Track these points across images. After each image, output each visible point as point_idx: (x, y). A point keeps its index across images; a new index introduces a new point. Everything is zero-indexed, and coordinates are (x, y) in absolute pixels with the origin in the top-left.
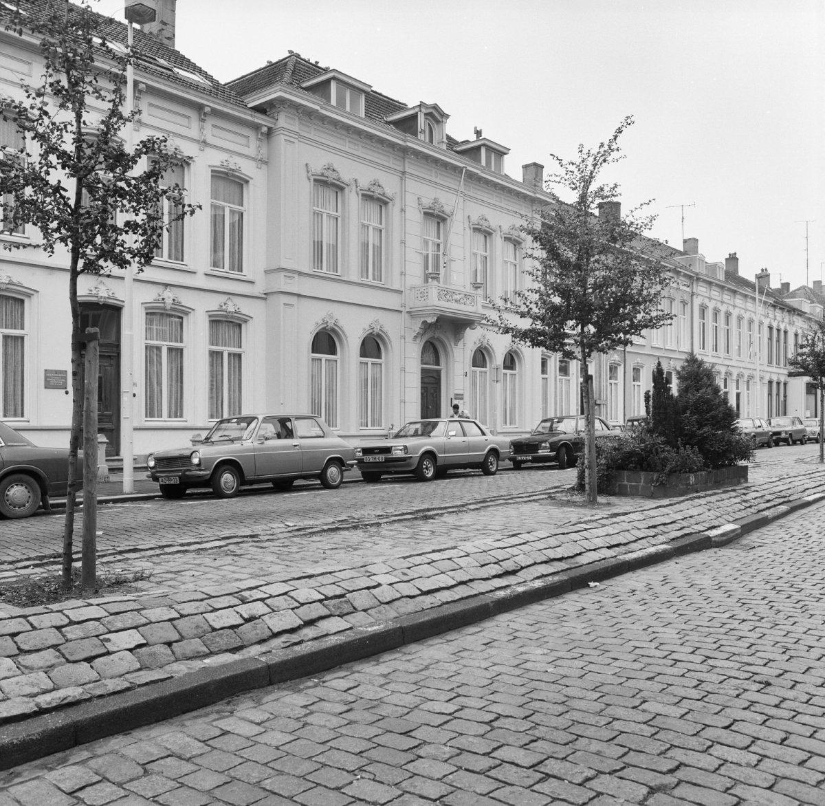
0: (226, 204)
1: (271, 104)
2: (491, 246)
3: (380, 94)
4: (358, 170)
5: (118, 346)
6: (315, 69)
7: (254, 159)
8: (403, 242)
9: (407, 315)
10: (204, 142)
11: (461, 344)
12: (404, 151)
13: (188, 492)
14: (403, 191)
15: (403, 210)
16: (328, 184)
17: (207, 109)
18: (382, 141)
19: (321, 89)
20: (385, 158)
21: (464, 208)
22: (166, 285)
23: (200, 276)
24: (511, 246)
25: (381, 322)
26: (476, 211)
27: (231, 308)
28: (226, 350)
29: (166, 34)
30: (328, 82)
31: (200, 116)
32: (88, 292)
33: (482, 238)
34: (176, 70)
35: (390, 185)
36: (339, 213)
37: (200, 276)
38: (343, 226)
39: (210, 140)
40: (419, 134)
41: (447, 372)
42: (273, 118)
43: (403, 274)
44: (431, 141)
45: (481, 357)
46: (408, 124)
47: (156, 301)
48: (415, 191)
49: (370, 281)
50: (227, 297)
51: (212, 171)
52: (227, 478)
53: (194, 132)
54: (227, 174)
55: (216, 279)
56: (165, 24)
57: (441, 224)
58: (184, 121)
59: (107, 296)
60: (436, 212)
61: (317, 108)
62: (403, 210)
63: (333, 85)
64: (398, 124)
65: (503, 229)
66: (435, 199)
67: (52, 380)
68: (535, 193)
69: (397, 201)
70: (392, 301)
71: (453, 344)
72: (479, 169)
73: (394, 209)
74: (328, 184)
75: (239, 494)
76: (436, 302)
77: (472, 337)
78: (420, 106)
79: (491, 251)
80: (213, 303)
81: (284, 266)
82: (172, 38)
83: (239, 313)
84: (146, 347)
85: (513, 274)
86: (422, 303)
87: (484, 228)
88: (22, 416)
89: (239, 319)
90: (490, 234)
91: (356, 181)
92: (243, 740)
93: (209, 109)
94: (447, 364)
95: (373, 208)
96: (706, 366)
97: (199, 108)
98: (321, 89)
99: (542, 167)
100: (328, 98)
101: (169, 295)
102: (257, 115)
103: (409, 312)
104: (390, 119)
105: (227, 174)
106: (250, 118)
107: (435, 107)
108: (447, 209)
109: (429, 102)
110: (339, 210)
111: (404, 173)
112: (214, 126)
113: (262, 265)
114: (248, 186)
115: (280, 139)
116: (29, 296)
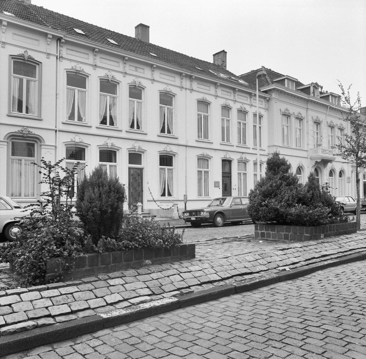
0: (202, 113)
1: (270, 90)
2: (290, 122)
3: (278, 73)
4: (295, 109)
5: (230, 173)
6: (278, 75)
7: (265, 109)
8: (308, 133)
9: (310, 159)
10: (95, 65)
11: (326, 168)
12: (308, 101)
13: (202, 224)
14: (307, 116)
15: (307, 122)
16: (287, 115)
17: (218, 84)
18: (301, 98)
19: (282, 82)
20: (301, 104)
21: (326, 118)
22: (243, 153)
23: (235, 147)
24: (330, 129)
25: (302, 162)
26: (329, 119)
27: (168, 150)
28: (203, 170)
29: (224, 65)
30: (284, 79)
31: (234, 91)
32: (70, 140)
33: (298, 121)
34: (239, 81)
35: (303, 113)
36: (289, 125)
37: (235, 147)
38: (290, 130)
39: (99, 64)
40: (311, 94)
41: (321, 179)
42: (270, 94)
43: (308, 144)
44: (314, 95)
45: (331, 173)
46: (306, 90)
47: (240, 158)
48: (312, 114)
49: (298, 148)
50: (166, 145)
51: (100, 79)
52: (219, 219)
53: (121, 69)
54: (225, 107)
55: (200, 142)
56: (224, 62)
57: (318, 126)
58: (86, 56)
59: (79, 141)
60: (318, 121)
61: (285, 90)
62: (307, 122)
63: (286, 80)
64: (302, 90)
65: (295, 113)
66: (317, 117)
67: (216, 185)
68: (309, 98)
69: (306, 118)
70: (304, 154)
71: (323, 167)
72: (285, 89)
73: (305, 121)
74: (287, 115)
75: (225, 225)
76: (321, 154)
77: (329, 165)
78: (311, 84)
79: (290, 124)
80: (101, 142)
81: (275, 145)
82: (225, 66)
83: (172, 151)
84: (238, 174)
85: (299, 132)
86: (316, 155)
87: (287, 114)
88: (208, 196)
89: (208, 158)
90: (289, 116)
91: (294, 113)
92: (170, 345)
93: (219, 84)
94: (321, 176)
95: (285, 118)
96: (281, 157)
97: (234, 89)
98: (282, 82)
99: (149, 27)
100: (284, 85)
101: (244, 156)
102: (264, 93)
103: (310, 158)
104: (298, 88)
105: (166, 93)
106: (264, 95)
107: (316, 84)
108: (321, 120)
109: (314, 82)
110: (289, 124)
111: (307, 108)
112: (130, 65)
113: (267, 145)
114: (231, 111)
115: (273, 102)
116: (87, 147)
